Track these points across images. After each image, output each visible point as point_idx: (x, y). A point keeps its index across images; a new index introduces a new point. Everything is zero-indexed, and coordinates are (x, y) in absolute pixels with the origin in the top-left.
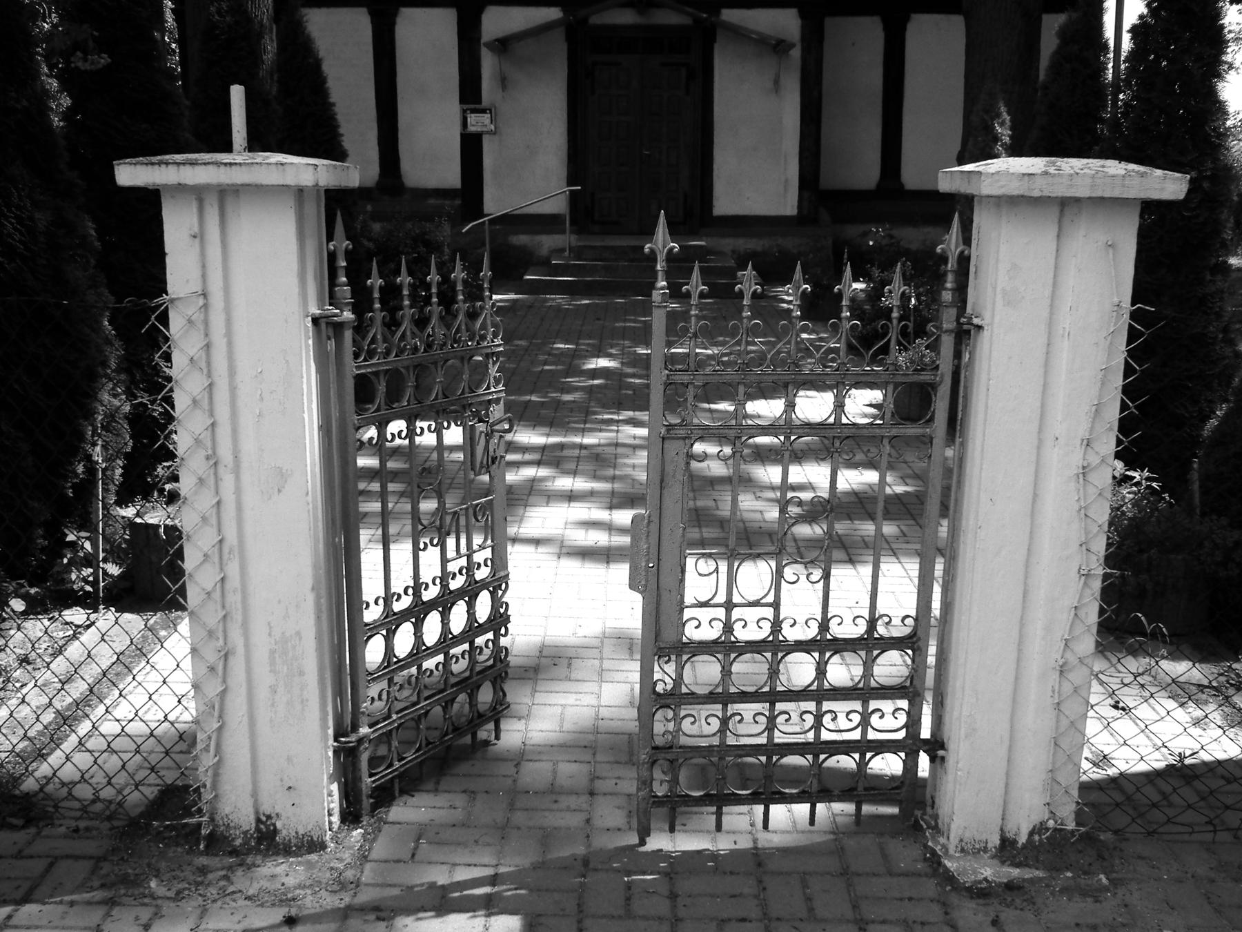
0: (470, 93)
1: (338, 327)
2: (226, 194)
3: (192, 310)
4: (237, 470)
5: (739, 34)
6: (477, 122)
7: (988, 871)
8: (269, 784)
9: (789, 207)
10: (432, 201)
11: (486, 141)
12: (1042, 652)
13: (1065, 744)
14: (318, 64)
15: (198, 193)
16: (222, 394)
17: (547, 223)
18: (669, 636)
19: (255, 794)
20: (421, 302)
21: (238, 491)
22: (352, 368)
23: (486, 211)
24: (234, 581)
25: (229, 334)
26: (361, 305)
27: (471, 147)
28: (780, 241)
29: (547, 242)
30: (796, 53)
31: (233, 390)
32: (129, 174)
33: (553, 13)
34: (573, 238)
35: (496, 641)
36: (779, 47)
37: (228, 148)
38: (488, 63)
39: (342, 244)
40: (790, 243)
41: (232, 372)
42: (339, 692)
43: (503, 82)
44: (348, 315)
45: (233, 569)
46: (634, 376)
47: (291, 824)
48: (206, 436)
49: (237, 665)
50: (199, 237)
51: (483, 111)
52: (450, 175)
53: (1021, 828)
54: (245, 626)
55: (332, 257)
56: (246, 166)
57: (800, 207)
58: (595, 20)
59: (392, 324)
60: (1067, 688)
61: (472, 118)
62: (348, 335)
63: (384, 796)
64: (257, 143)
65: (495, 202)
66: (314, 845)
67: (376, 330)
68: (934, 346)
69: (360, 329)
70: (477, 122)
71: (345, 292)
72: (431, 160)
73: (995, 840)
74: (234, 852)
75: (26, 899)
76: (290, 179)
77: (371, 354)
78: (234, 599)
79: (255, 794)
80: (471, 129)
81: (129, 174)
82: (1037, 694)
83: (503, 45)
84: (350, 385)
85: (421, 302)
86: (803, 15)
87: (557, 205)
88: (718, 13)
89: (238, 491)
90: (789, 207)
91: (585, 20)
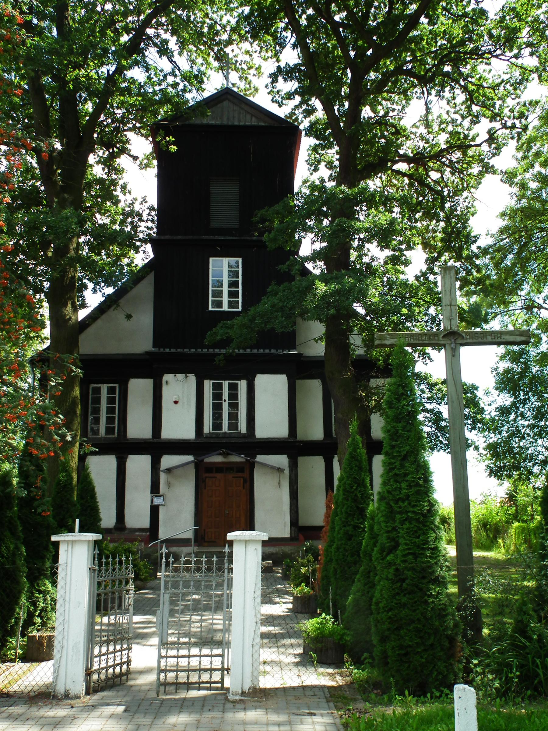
0: (155, 488)
1: (95, 570)
2: (73, 542)
3: (64, 567)
4: (69, 603)
5: (264, 465)
6: (157, 501)
7: (237, 698)
8: (69, 682)
9: (286, 533)
10: (137, 533)
11: (161, 509)
12: (248, 643)
13: (255, 665)
14: (93, 488)
15: (68, 542)
16: (68, 585)
17: (185, 542)
18: (164, 641)
19: (65, 684)
20: (114, 564)
21: (69, 608)
22: (97, 580)
23: (160, 537)
24: (66, 629)
25: (71, 572)
26: (100, 565)
27: (155, 511)
28: (283, 548)
29: (185, 550)
30: (287, 472)
31: (70, 584)
32: (54, 538)
33: (190, 458)
34: (196, 548)
35: (128, 654)
36: (280, 470)
37: (74, 532)
38: (163, 477)
39: (97, 552)
40: (287, 549)
41: (71, 580)
42: (87, 660)
43: (169, 485)
44: (97, 568)
45: (66, 626)
46: (204, 601)
47: (72, 693)
48: (63, 595)
49: (65, 649)
50: (67, 551)
51: (160, 496)
52: (146, 523)
53: (246, 689)
54: (67, 640)
55: (94, 555)
56: (78, 536)
57: (291, 534)
58: (207, 460)
59: (107, 570)
60: (254, 651)
61: (155, 499)
62: (97, 572)
63: (96, 691)
64: (80, 531)
65: (163, 533)
66: (78, 697)
67: (103, 571)
68: (224, 572)
69: (100, 571)
70: (157, 501)
71: (96, 562)
72: (137, 516)
73: (240, 692)
74: (59, 699)
75: (11, 706)
76: (87, 539)
77: (101, 577)
78: (66, 633)
79: (65, 684)
80: (155, 503)
81: (54, 538)
82: (248, 651)
83: (169, 471)
84: (96, 583)
85: (114, 564)
86: (289, 457)
87: (190, 535)
88: (255, 457)
89: (69, 608)
90: (286, 533)
91: (203, 460)
